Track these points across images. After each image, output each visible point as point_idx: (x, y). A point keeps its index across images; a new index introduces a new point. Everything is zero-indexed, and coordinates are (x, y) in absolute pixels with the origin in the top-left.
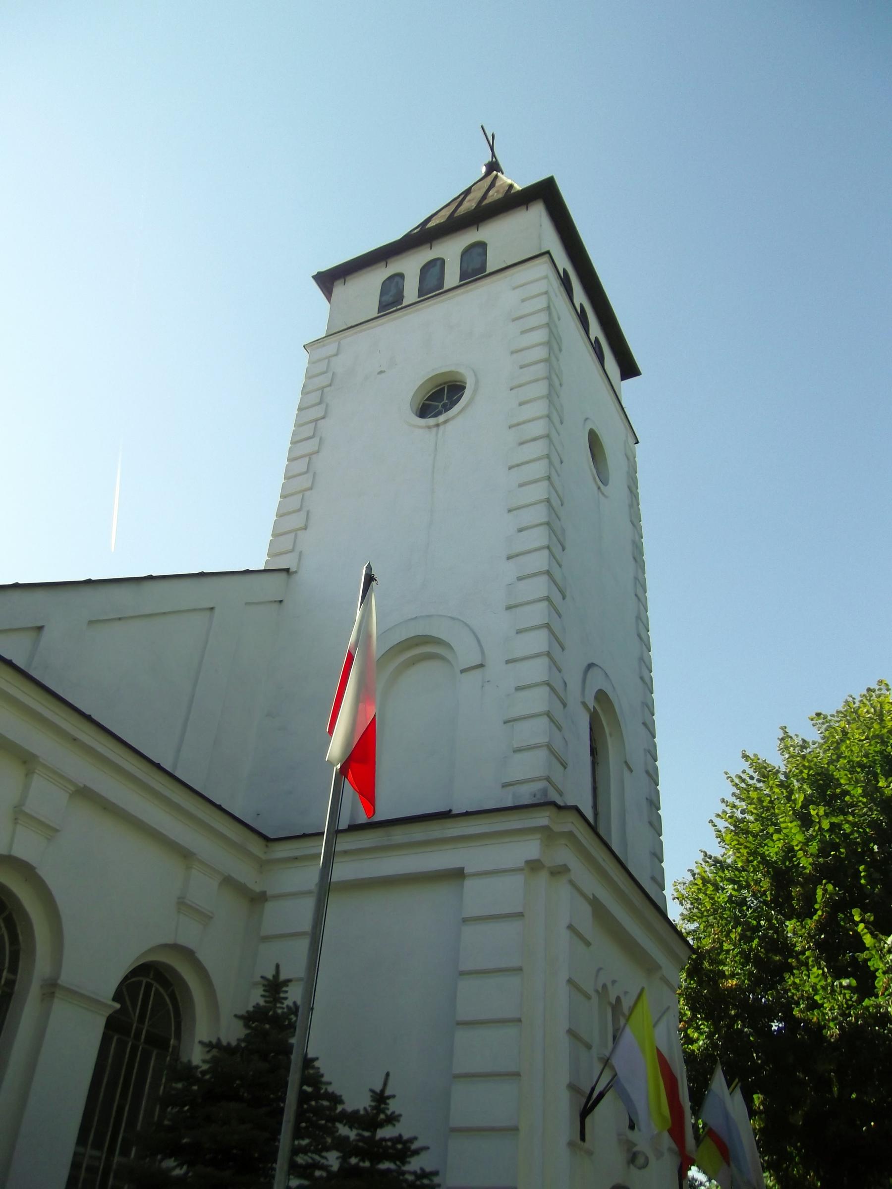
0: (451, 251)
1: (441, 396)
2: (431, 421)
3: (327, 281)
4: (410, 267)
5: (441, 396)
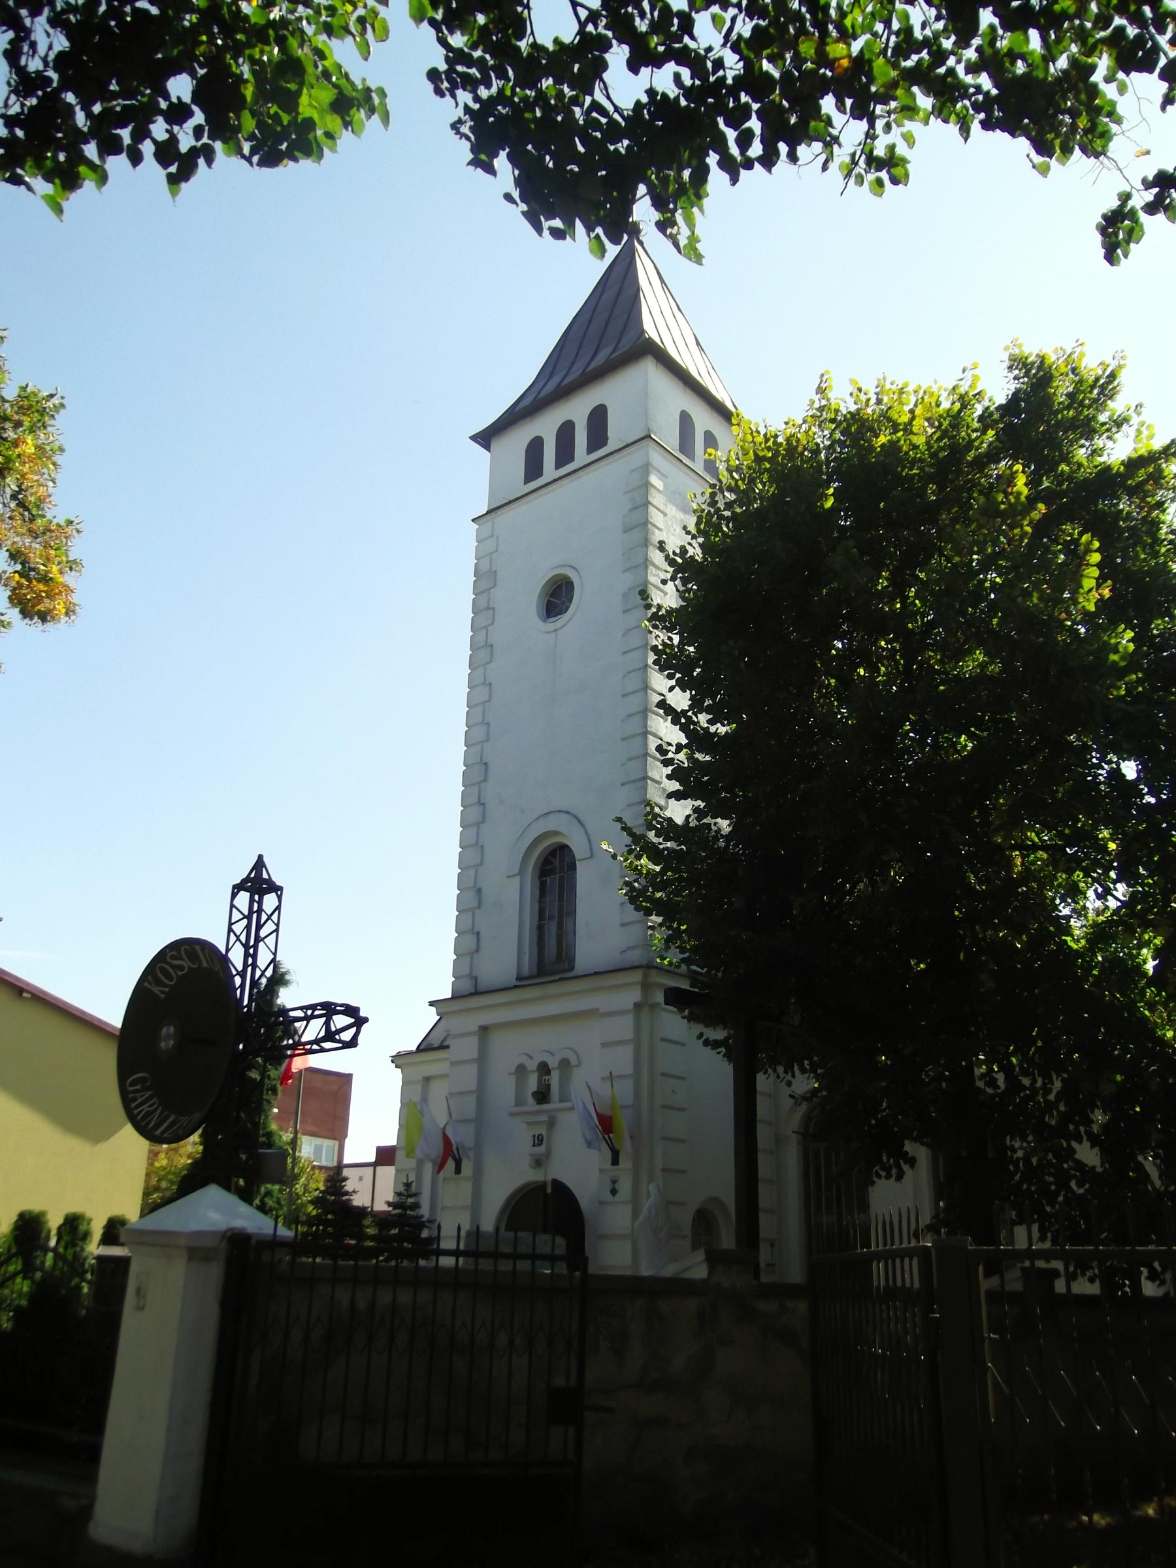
0: (577, 409)
1: (557, 597)
2: (550, 626)
3: (485, 438)
4: (546, 426)
5: (557, 597)
